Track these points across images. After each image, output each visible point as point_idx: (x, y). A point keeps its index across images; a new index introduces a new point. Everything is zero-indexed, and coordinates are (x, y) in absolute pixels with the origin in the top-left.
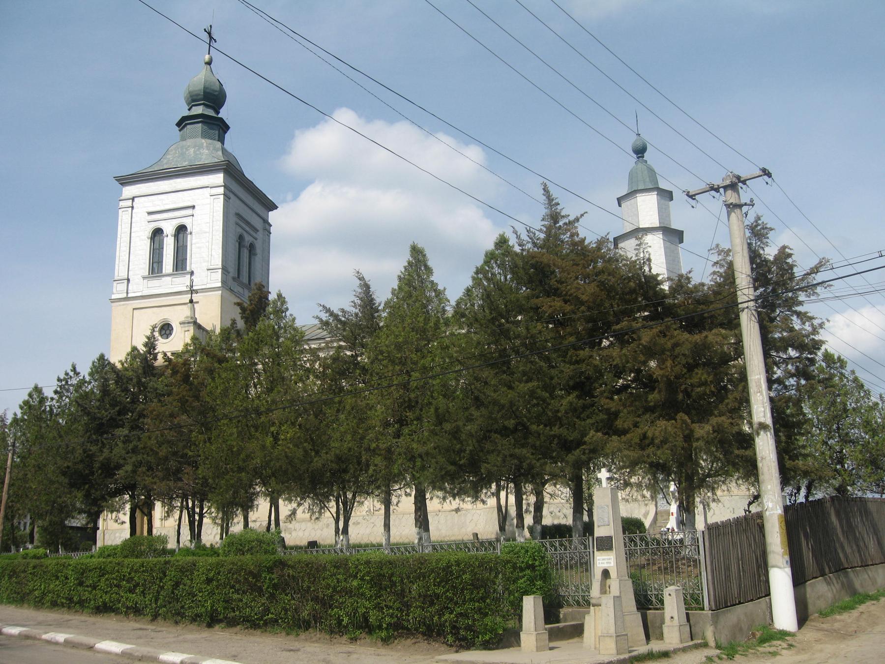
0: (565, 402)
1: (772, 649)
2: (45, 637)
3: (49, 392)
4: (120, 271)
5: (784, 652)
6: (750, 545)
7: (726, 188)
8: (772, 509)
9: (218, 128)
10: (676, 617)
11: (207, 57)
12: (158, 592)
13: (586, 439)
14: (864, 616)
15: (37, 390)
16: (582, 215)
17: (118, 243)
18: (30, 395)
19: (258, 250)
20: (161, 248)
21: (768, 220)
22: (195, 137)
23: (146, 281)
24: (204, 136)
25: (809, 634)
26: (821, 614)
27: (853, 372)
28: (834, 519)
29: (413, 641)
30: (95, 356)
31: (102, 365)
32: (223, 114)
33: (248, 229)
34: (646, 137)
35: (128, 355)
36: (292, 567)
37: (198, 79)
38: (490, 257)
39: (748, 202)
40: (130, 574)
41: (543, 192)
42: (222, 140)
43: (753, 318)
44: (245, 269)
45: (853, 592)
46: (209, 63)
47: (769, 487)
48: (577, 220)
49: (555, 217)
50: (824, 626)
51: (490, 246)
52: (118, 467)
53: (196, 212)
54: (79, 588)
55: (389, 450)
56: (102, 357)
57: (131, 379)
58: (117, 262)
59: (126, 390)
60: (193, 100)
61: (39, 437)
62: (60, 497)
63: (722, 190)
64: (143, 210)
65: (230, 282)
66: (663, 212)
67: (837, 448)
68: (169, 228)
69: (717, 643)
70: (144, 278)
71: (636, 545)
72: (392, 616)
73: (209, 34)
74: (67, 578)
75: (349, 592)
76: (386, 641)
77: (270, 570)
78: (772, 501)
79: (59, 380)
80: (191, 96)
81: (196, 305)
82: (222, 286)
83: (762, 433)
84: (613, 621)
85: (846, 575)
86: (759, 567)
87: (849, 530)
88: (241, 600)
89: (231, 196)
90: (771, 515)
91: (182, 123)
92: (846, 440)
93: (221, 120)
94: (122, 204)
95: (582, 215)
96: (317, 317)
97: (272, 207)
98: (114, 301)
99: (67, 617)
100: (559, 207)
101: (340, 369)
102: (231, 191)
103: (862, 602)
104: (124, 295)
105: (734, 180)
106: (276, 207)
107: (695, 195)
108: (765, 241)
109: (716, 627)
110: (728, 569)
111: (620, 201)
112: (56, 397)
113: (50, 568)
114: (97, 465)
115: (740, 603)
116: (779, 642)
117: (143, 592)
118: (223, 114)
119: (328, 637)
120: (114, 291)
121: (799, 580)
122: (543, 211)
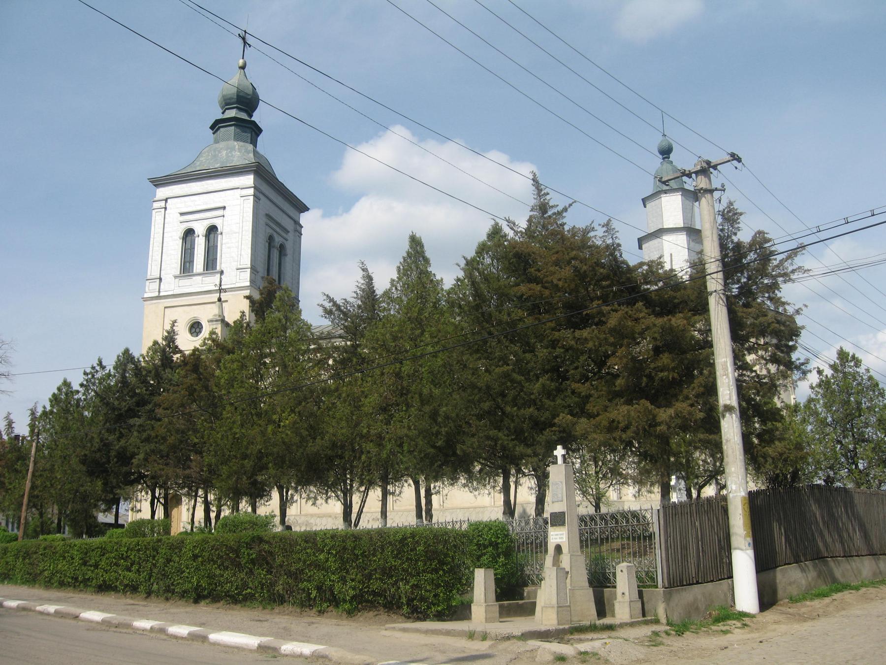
0: (538, 385)
1: (724, 628)
2: (39, 608)
3: (76, 386)
5: (737, 630)
6: (712, 527)
7: (697, 173)
8: (735, 492)
10: (627, 594)
11: (241, 62)
12: (151, 570)
13: (556, 421)
14: (835, 603)
15: (66, 384)
16: (570, 205)
17: (151, 242)
18: (59, 389)
20: (192, 248)
21: (738, 206)
22: (228, 140)
23: (177, 280)
24: (237, 138)
25: (770, 615)
26: (791, 599)
27: (868, 370)
28: (814, 508)
29: (376, 613)
30: (120, 351)
31: (127, 358)
32: (256, 117)
33: (278, 230)
35: (149, 349)
36: (267, 542)
37: (235, 79)
38: (482, 249)
39: (719, 187)
40: (127, 552)
42: (254, 143)
43: (721, 302)
45: (834, 580)
46: (243, 68)
47: (733, 469)
48: (565, 210)
49: (543, 208)
50: (791, 610)
51: (483, 237)
52: (133, 455)
53: (226, 213)
54: (83, 568)
55: (380, 437)
56: (127, 351)
57: (150, 372)
58: (150, 262)
59: (145, 382)
60: (227, 104)
61: (65, 429)
62: (82, 486)
63: (694, 176)
64: (174, 212)
66: (688, 213)
67: (851, 447)
68: (200, 229)
69: (668, 621)
70: (176, 277)
71: (596, 524)
72: (354, 589)
73: (245, 42)
74: (73, 559)
75: (318, 566)
76: (350, 613)
77: (249, 546)
78: (736, 484)
79: (85, 374)
80: (225, 100)
81: (224, 304)
82: (251, 286)
83: (727, 415)
84: (554, 592)
85: (826, 564)
86: (721, 548)
87: (832, 520)
88: (222, 576)
89: (261, 196)
90: (735, 497)
91: (216, 126)
92: (861, 439)
93: (254, 123)
94: (156, 205)
95: (570, 205)
96: (322, 306)
97: (303, 208)
98: (146, 300)
99: (71, 595)
100: (548, 197)
101: (350, 360)
103: (838, 590)
104: (156, 294)
105: (705, 165)
106: (307, 209)
107: (667, 181)
108: (736, 226)
109: (668, 604)
110: (685, 548)
111: (644, 201)
112: (81, 390)
113: (58, 548)
114: (113, 453)
115: (698, 583)
116: (734, 622)
117: (138, 570)
118: (256, 117)
119: (298, 610)
121: (765, 564)
122: (532, 201)
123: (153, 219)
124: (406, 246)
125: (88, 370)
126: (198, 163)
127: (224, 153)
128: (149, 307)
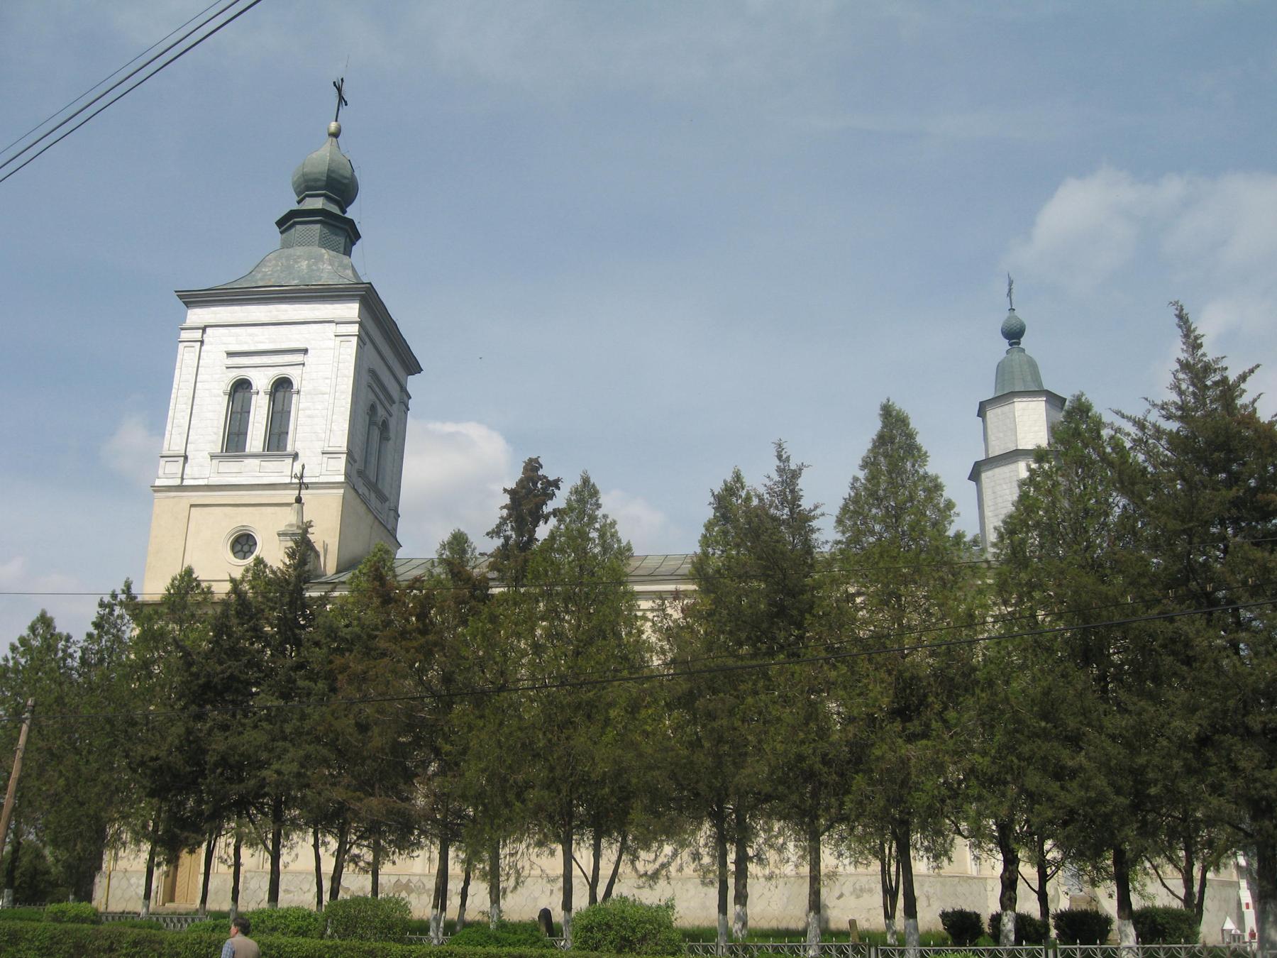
4: (173, 441)
9: (345, 234)
11: (333, 126)
16: (1252, 371)
18: (33, 629)
19: (392, 434)
22: (309, 244)
23: (215, 462)
24: (324, 243)
30: (177, 570)
32: (351, 213)
33: (382, 397)
34: (1022, 315)
37: (321, 156)
41: (1176, 320)
42: (348, 252)
44: (373, 460)
46: (336, 135)
64: (212, 353)
65: (354, 474)
68: (262, 381)
70: (213, 457)
80: (306, 181)
91: (286, 222)
94: (185, 335)
95: (1252, 371)
102: (367, 334)
104: (178, 482)
111: (982, 411)
118: (351, 213)
120: (160, 472)
123: (179, 357)
124: (874, 426)
125: (107, 599)
126: (259, 276)
127: (304, 264)
128: (163, 503)
